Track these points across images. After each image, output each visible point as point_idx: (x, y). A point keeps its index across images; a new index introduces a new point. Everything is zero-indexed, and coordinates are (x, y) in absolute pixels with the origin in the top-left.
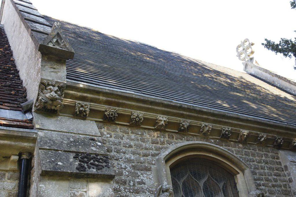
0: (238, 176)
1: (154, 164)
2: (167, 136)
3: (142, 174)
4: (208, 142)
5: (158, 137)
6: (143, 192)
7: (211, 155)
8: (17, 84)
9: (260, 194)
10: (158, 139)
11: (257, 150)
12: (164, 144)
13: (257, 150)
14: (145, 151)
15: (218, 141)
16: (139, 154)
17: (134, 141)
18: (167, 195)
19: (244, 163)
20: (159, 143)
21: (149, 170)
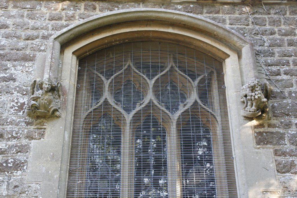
0: (228, 61)
1: (44, 50)
2: (83, 7)
3: (14, 66)
4: (172, 9)
5: (63, 9)
6: (7, 93)
7: (170, 30)
8: (186, 45)
9: (255, 85)
10: (63, 13)
11: (288, 13)
12: (73, 19)
13: (288, 13)
14: (30, 33)
15: (192, 6)
16: (18, 37)
17: (15, 18)
18: (39, 94)
19: (238, 37)
20: (64, 18)
21: (31, 59)
